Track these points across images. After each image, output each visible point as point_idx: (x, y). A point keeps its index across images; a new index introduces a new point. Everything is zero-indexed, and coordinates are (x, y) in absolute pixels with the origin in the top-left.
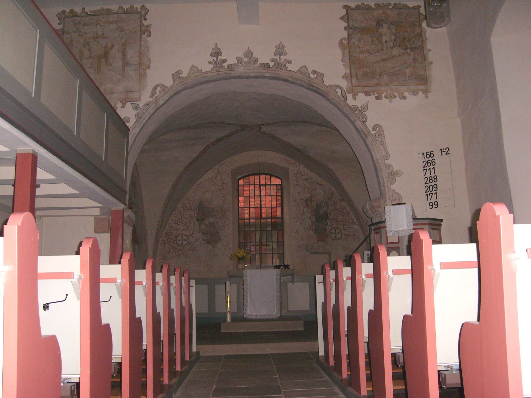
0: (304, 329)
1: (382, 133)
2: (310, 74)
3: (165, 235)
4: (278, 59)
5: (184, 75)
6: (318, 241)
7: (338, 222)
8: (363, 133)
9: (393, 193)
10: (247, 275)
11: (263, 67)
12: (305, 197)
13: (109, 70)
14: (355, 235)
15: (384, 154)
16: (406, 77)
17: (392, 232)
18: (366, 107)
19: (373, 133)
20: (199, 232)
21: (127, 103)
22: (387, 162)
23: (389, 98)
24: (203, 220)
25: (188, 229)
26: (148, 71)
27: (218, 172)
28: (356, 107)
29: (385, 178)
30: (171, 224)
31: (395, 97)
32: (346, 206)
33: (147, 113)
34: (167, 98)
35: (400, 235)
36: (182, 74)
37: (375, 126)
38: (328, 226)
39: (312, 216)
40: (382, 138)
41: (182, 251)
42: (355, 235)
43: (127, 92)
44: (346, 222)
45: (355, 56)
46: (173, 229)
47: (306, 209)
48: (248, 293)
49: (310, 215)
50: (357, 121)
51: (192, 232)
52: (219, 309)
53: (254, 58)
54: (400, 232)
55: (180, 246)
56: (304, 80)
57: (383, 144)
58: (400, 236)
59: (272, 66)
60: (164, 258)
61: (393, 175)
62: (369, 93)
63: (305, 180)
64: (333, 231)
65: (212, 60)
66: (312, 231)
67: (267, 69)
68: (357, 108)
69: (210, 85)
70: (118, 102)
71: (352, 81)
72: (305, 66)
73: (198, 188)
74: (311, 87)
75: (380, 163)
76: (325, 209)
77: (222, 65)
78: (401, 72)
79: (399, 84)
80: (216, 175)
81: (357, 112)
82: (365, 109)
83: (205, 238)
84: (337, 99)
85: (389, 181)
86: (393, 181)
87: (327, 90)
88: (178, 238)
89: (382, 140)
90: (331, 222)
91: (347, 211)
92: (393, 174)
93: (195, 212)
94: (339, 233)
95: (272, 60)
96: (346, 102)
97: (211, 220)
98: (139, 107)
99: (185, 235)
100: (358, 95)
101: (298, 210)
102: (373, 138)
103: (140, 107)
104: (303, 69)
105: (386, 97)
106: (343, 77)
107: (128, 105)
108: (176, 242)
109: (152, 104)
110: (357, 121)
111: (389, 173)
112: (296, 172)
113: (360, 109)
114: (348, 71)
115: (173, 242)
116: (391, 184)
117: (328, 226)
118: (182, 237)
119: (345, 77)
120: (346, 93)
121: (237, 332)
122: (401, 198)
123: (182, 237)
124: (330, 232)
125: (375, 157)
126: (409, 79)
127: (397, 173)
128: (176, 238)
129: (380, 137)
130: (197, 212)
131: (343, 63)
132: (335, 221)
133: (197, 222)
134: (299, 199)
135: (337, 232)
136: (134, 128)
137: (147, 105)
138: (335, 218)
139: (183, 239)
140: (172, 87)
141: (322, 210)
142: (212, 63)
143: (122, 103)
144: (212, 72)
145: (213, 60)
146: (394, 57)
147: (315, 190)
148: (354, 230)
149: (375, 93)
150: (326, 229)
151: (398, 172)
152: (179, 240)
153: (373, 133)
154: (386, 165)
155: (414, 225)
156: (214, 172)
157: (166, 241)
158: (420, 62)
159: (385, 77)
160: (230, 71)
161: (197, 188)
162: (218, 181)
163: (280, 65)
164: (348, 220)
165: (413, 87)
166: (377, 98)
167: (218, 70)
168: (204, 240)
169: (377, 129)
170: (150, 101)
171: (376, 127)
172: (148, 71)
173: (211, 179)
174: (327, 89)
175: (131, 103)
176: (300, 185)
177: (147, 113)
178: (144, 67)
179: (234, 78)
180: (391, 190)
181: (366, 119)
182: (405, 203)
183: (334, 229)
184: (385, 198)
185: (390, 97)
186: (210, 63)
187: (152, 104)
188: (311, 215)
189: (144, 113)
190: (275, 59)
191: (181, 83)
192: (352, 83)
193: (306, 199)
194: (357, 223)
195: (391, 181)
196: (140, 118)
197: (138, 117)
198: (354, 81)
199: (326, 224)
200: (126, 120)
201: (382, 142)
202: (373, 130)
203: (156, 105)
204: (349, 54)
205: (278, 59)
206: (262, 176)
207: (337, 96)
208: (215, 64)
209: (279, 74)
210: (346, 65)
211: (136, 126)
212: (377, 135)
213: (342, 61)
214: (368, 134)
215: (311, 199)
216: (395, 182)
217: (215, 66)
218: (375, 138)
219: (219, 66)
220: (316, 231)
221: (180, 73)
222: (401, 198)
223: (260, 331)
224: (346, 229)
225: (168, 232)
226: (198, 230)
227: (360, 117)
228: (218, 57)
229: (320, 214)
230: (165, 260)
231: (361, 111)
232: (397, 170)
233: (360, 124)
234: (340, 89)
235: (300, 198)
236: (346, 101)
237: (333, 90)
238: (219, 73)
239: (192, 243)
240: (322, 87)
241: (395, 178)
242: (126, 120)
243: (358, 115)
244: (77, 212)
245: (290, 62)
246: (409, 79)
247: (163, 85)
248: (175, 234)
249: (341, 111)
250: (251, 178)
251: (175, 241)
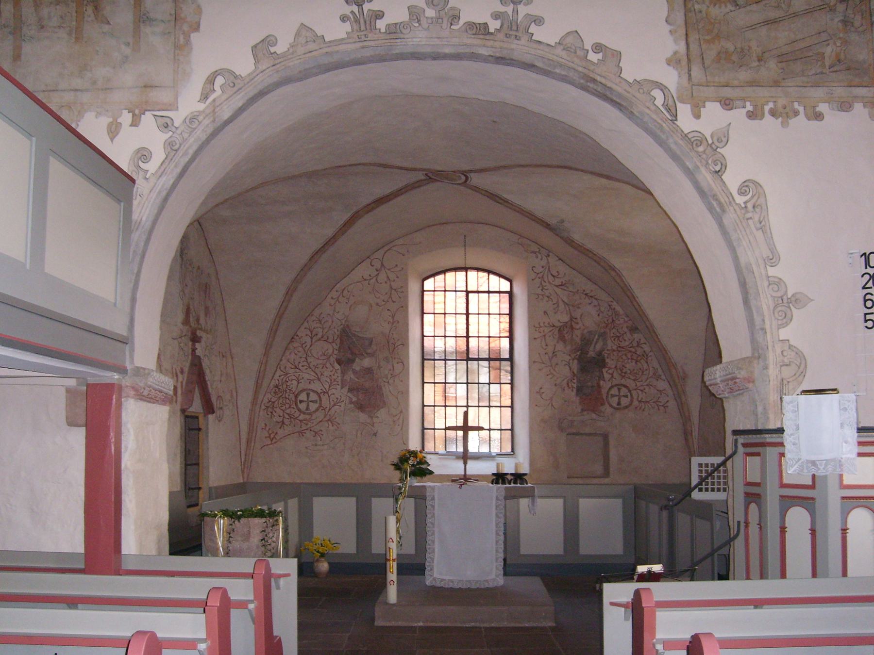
0: (554, 625)
1: (761, 201)
2: (588, 52)
3: (274, 390)
4: (510, 13)
5: (280, 48)
6: (583, 410)
7: (625, 373)
8: (717, 200)
9: (785, 348)
10: (434, 496)
11: (474, 32)
12: (559, 321)
13: (103, 33)
14: (660, 402)
15: (766, 253)
16: (823, 66)
17: (800, 462)
18: (723, 137)
19: (740, 200)
20: (342, 388)
21: (144, 114)
22: (772, 271)
23: (781, 116)
24: (351, 361)
25: (319, 379)
26: (194, 36)
27: (382, 265)
28: (699, 135)
29: (766, 313)
30: (285, 368)
31: (796, 113)
32: (642, 342)
33: (192, 140)
34: (240, 104)
35: (820, 473)
36: (275, 45)
37: (746, 184)
38: (604, 381)
39: (571, 361)
40: (763, 215)
41: (307, 424)
42: (660, 402)
43: (145, 87)
44: (640, 373)
45: (700, 12)
46: (290, 378)
47: (560, 346)
48: (436, 534)
49: (568, 358)
50: (703, 169)
51: (327, 387)
52: (377, 548)
53: (452, 8)
54: (821, 465)
55: (304, 413)
56: (572, 65)
57: (763, 227)
58: (822, 474)
59: (496, 29)
60: (272, 436)
61: (787, 305)
62: (731, 103)
63: (560, 286)
64: (614, 391)
65: (348, 13)
66: (572, 391)
67: (482, 37)
68: (701, 140)
69: (345, 75)
70: (124, 111)
71: (690, 70)
72: (576, 31)
73: (341, 296)
74: (591, 85)
75: (756, 274)
76: (599, 347)
77: (373, 23)
78: (811, 54)
79: (807, 82)
80: (377, 270)
81: (701, 149)
82: (722, 141)
83: (354, 399)
84: (654, 116)
85: (775, 319)
86: (786, 319)
87: (628, 92)
88: (301, 398)
89: (761, 219)
90: (609, 374)
91: (644, 352)
92: (785, 301)
93: (334, 344)
94: (626, 396)
95: (496, 16)
96: (674, 123)
97: (367, 362)
98: (173, 125)
99: (313, 391)
100: (704, 107)
101: (545, 347)
102: (739, 213)
103: (175, 125)
104: (570, 40)
105: (773, 113)
106: (669, 62)
107: (148, 119)
108: (296, 405)
109: (204, 118)
110: (703, 169)
111: (776, 299)
112: (542, 269)
113: (710, 141)
114: (682, 47)
115: (290, 406)
116: (779, 327)
117: (604, 381)
118: (308, 395)
119: (673, 61)
120: (675, 102)
121: (409, 627)
122: (803, 362)
123: (308, 395)
124: (608, 393)
125: (743, 260)
126: (830, 72)
127: (798, 300)
128: (296, 397)
129: (757, 210)
130: (338, 346)
131: (669, 28)
132: (619, 370)
133: (337, 366)
134: (546, 324)
135: (622, 394)
136: (160, 176)
137: (192, 119)
138: (618, 367)
139: (310, 399)
140: (252, 77)
141: (591, 348)
142: (349, 19)
143: (133, 115)
144: (351, 41)
145: (352, 12)
146: (795, 15)
147: (579, 308)
148: (658, 390)
149: (748, 104)
150: (599, 386)
151: (798, 296)
152: (301, 402)
153: (740, 200)
154: (771, 279)
155: (860, 444)
156: (373, 266)
157: (277, 402)
158: (861, 29)
159: (772, 64)
160: (392, 41)
161: (339, 296)
162: (381, 283)
163: (514, 28)
164: (647, 370)
165: (840, 92)
166: (750, 116)
167: (363, 38)
168: (351, 402)
169: (751, 193)
170: (199, 111)
171: (747, 186)
172: (194, 36)
173: (365, 280)
174: (629, 90)
175: (155, 116)
176: (548, 297)
177: (193, 139)
178: (185, 28)
179: (402, 57)
180: (780, 341)
181: (724, 166)
182: (835, 390)
183: (616, 388)
184: (765, 359)
185: (784, 114)
186: (344, 19)
187: (204, 118)
188: (570, 358)
189: (185, 140)
190: (501, 12)
191: (274, 67)
192: (690, 75)
193: (562, 324)
194: (663, 377)
195: (780, 318)
196: (176, 150)
197: (169, 149)
198: (697, 72)
199: (601, 377)
200: (143, 155)
201: (760, 223)
202: (741, 193)
203: (214, 121)
204: (685, 6)
205: (510, 13)
206: (472, 274)
207: (653, 108)
208: (356, 21)
209: (512, 49)
210: (676, 32)
211: (164, 170)
212: (750, 206)
213: (666, 21)
214: (728, 203)
215: (572, 326)
216: (791, 320)
217: (356, 27)
218: (744, 214)
219: (366, 27)
220: (579, 390)
221: (271, 42)
222: (803, 362)
223: (459, 625)
224: (642, 388)
225: (280, 384)
226: (340, 383)
227: (710, 162)
228: (364, 6)
229: (588, 356)
230: (274, 441)
231: (711, 147)
232: (796, 293)
233: (709, 177)
234: (662, 90)
235: (549, 324)
236: (676, 120)
237: (644, 93)
238: (365, 44)
239: (328, 408)
240: (616, 84)
241: (792, 313)
242: (143, 155)
243: (704, 156)
244: (12, 380)
245: (538, 21)
246: (830, 72)
247: (231, 72)
248: (294, 390)
249: (662, 143)
250: (450, 276)
251: (294, 405)
